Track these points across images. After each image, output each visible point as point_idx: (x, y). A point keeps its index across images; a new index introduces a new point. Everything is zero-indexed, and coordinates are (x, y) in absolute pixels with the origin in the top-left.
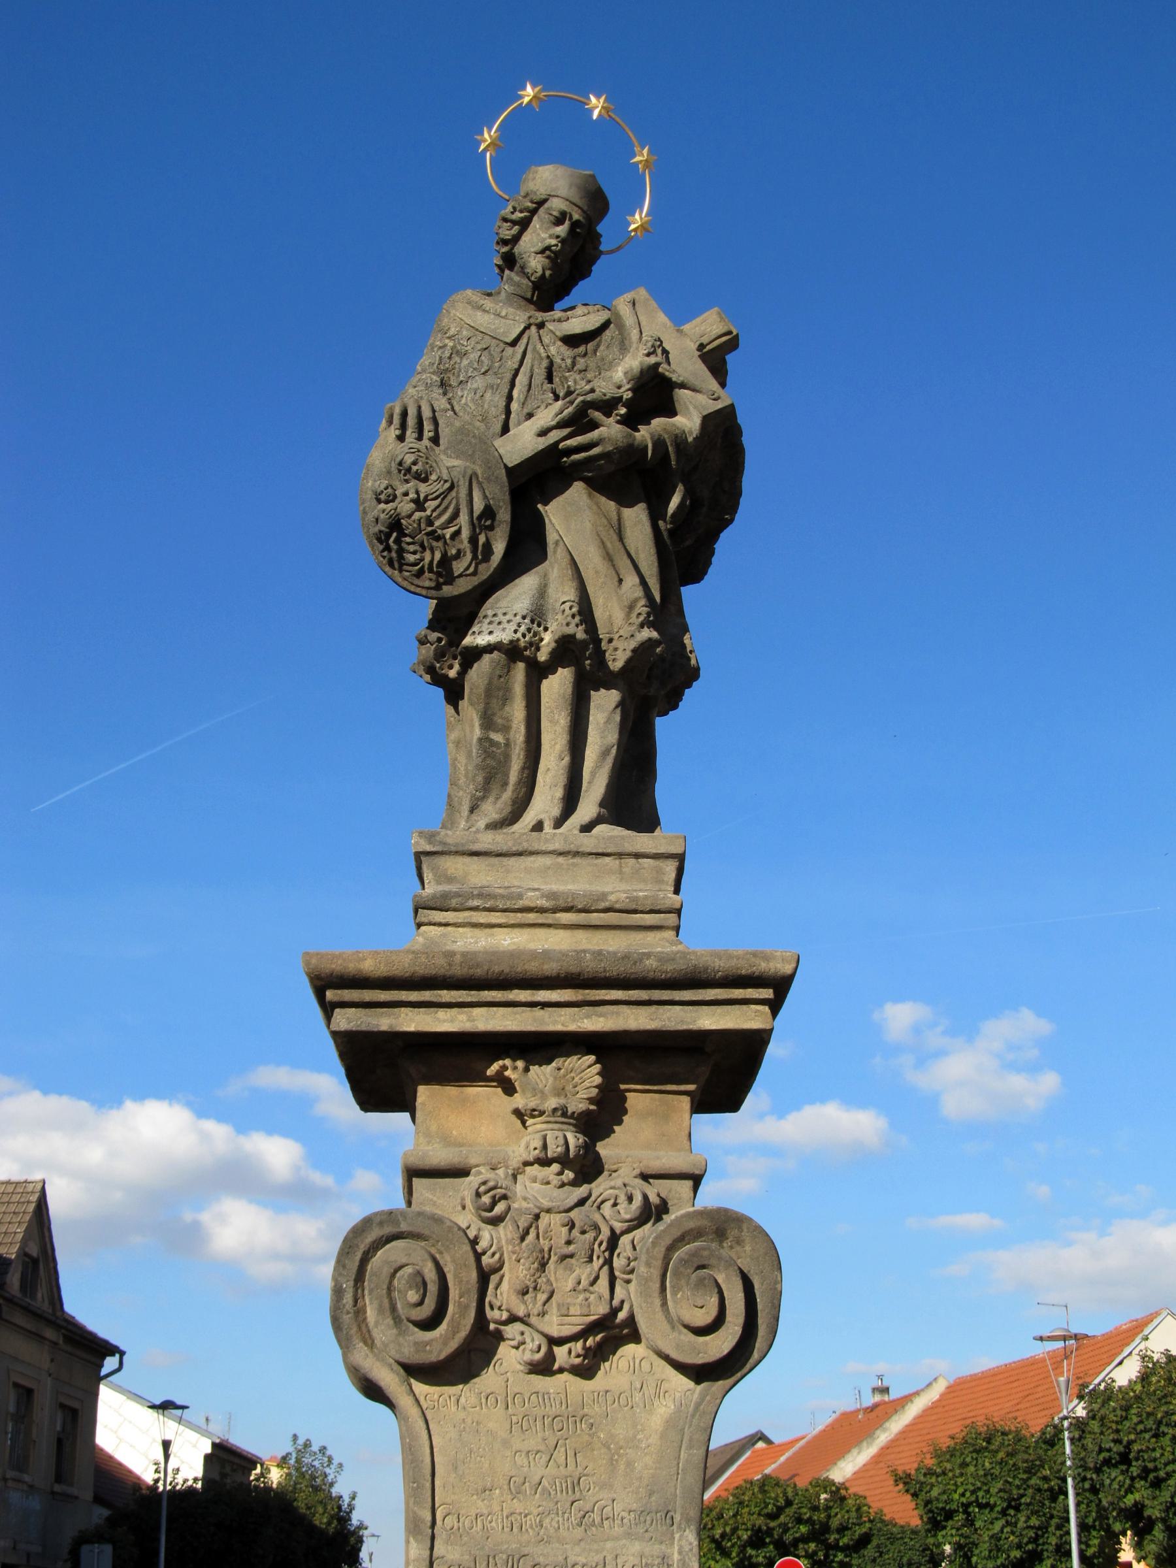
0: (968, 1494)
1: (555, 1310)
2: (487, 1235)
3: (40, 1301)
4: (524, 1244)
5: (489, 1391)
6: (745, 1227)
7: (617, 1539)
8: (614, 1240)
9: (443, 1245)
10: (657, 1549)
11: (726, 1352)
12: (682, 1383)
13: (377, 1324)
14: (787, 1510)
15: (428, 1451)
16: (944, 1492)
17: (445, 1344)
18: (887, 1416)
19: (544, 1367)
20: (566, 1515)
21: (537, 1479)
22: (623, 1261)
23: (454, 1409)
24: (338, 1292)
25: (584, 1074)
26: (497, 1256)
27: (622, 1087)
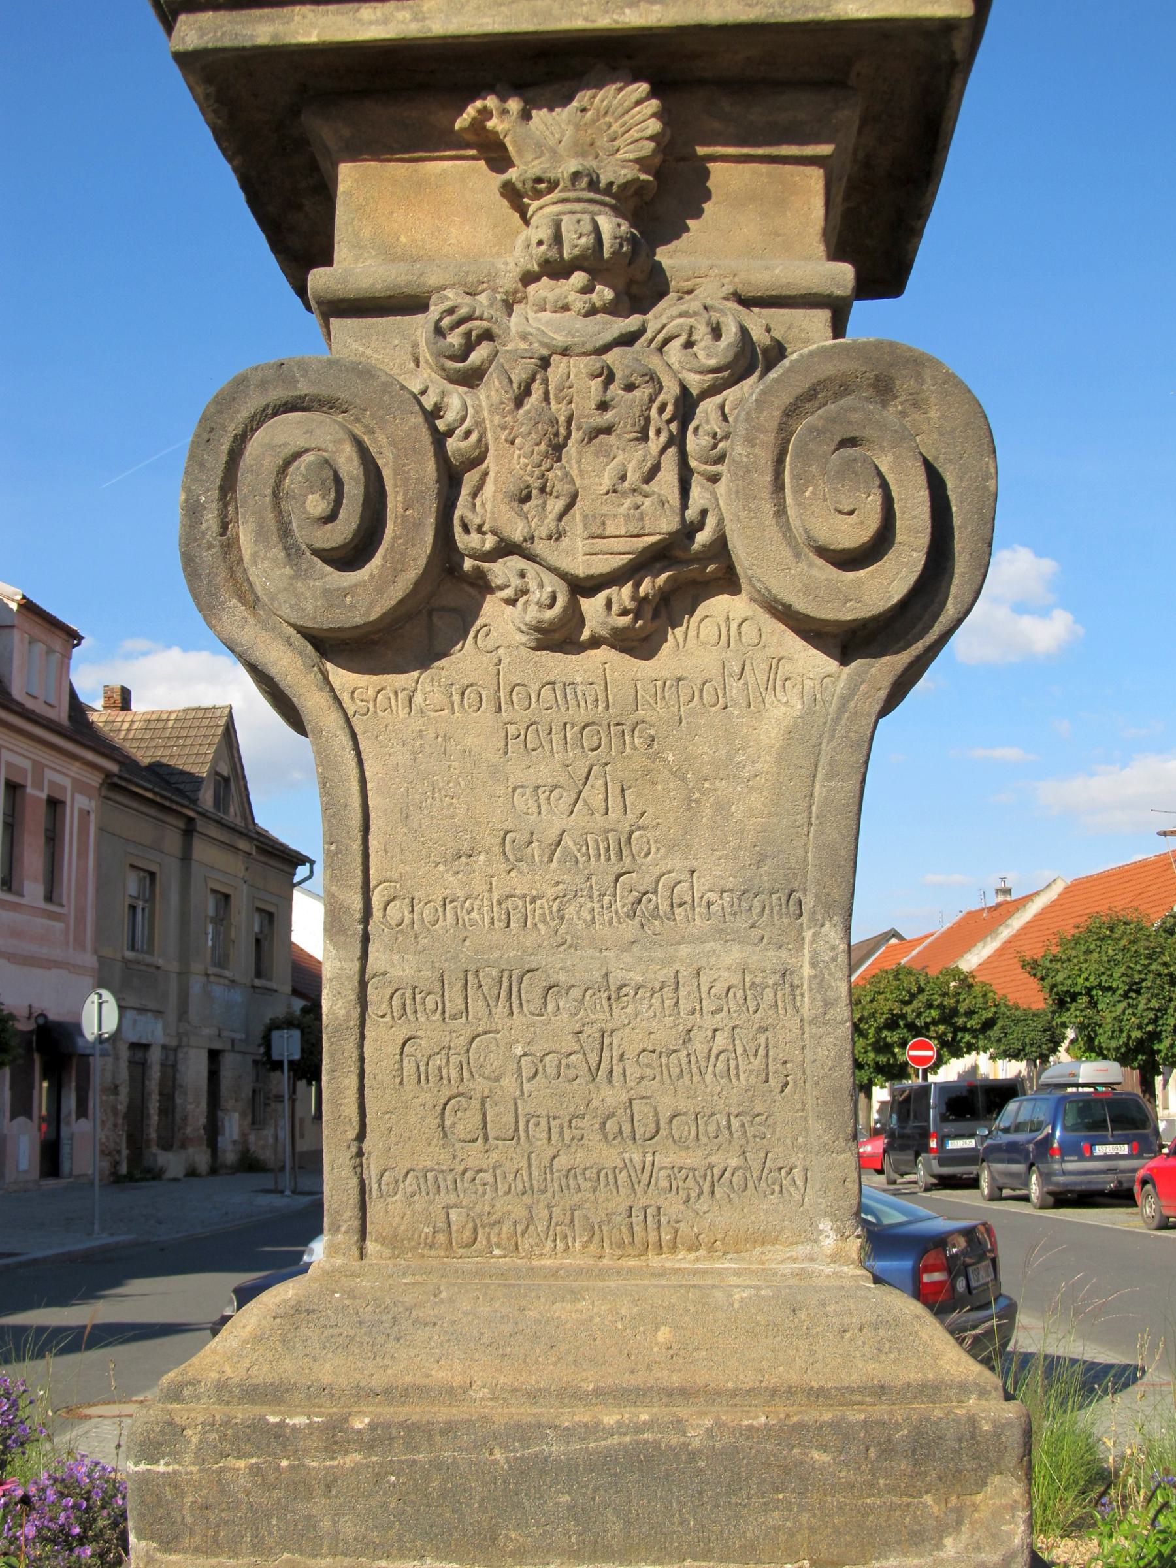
0: (1092, 978)
1: (580, 530)
2: (455, 400)
3: (233, 815)
4: (521, 412)
5: (465, 682)
6: (928, 374)
7: (700, 940)
8: (686, 406)
9: (373, 416)
10: (773, 957)
11: (896, 599)
12: (814, 663)
13: (255, 555)
14: (920, 997)
15: (355, 787)
16: (1069, 977)
17: (379, 591)
18: (1010, 914)
19: (561, 636)
20: (606, 899)
21: (552, 835)
22: (705, 440)
23: (402, 713)
24: (193, 511)
25: (623, 121)
26: (474, 437)
27: (701, 151)
